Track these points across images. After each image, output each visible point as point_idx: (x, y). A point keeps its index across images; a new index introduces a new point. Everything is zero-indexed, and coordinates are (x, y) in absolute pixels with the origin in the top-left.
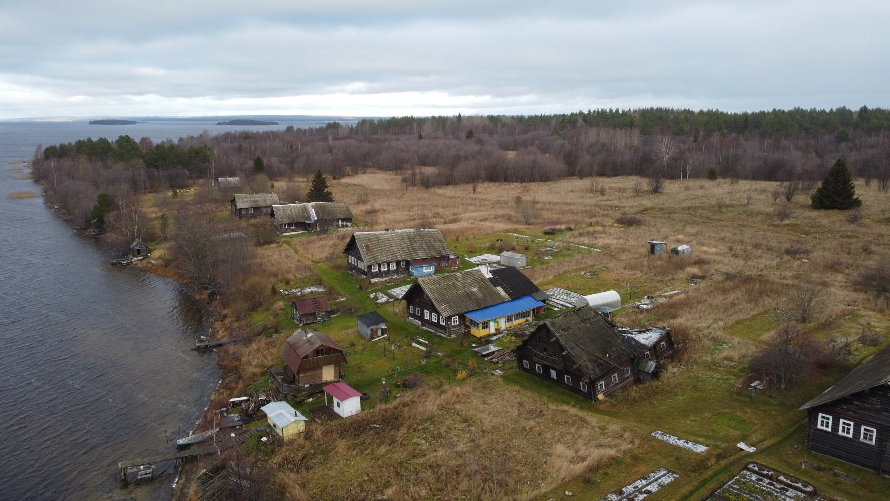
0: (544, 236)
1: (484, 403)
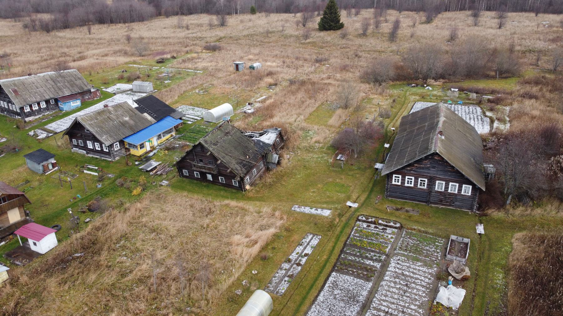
0: (157, 64)
1: (162, 211)
